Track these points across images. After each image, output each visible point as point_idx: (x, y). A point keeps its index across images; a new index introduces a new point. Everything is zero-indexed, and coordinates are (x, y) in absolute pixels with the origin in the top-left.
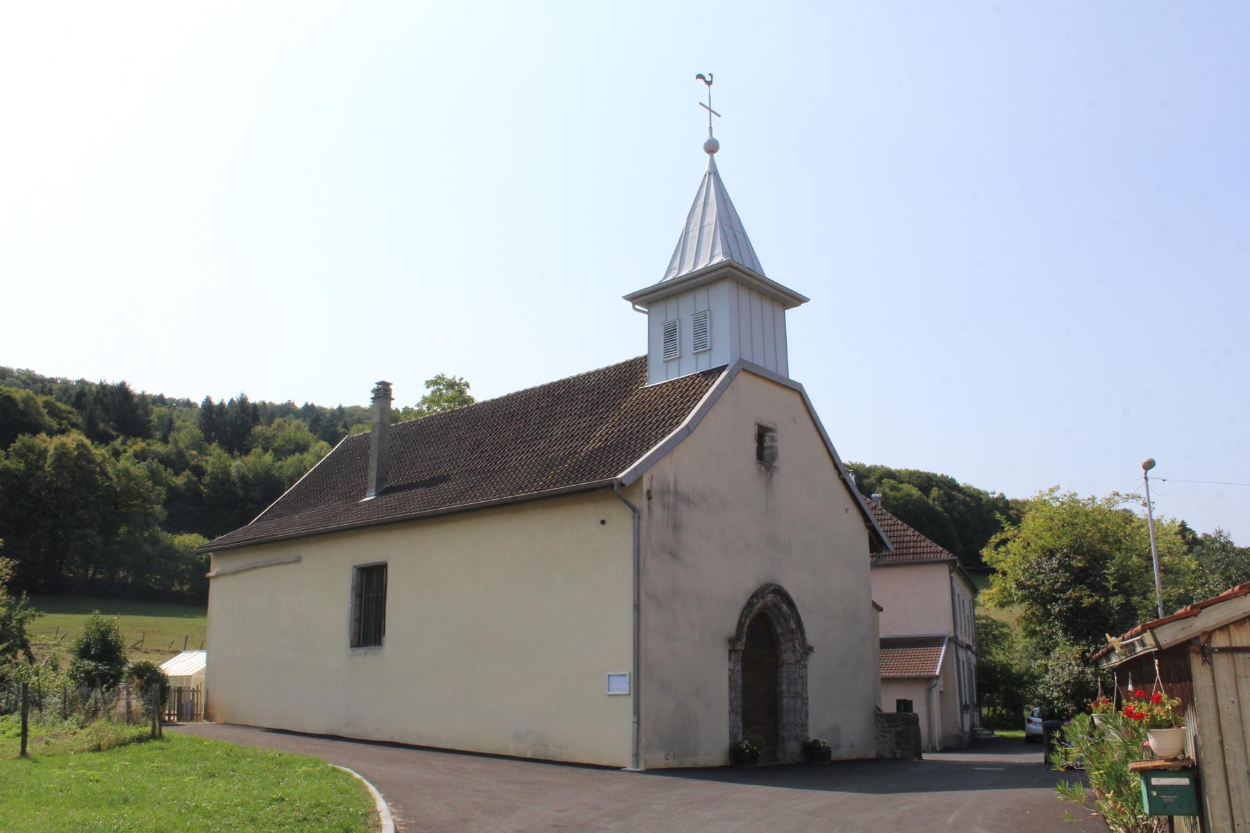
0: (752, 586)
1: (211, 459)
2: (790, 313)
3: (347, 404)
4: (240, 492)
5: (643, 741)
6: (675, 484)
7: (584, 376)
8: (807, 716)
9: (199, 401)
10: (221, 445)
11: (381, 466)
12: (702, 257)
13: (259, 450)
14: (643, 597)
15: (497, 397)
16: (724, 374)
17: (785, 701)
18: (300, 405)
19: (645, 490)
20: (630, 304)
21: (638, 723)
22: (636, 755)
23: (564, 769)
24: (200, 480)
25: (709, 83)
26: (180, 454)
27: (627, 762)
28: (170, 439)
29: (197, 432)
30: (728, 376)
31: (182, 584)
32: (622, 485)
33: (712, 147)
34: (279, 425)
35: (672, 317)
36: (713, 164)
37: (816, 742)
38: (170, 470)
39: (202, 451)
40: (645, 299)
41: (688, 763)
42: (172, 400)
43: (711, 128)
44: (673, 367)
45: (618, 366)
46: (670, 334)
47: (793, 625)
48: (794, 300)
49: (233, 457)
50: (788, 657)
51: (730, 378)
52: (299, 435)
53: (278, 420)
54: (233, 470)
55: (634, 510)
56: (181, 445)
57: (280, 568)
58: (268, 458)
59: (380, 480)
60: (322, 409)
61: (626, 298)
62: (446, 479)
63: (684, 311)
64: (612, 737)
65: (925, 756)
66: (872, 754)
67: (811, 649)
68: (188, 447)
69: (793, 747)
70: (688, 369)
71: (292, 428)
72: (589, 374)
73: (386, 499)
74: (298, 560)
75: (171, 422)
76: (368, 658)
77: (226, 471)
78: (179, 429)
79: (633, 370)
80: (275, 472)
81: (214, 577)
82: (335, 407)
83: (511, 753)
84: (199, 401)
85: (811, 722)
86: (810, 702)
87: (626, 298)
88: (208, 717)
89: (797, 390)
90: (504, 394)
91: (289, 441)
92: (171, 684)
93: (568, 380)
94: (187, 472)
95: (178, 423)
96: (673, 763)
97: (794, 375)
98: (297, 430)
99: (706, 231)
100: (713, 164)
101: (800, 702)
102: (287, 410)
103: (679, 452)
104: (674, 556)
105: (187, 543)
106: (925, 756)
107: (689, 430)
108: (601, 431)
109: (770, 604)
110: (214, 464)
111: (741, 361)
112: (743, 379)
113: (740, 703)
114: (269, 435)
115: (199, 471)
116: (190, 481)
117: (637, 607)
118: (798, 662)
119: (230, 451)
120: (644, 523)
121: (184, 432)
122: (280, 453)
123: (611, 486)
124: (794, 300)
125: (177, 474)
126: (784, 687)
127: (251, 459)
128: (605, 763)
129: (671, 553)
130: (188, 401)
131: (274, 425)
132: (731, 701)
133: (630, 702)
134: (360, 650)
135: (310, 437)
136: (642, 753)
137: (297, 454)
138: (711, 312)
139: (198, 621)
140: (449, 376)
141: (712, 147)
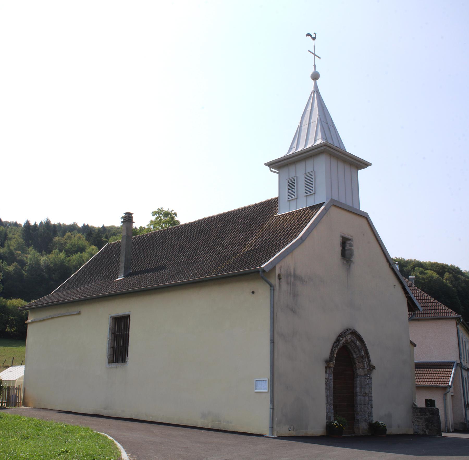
0: (338, 329)
1: (29, 256)
2: (361, 173)
3: (107, 225)
4: (46, 275)
5: (276, 419)
7: (242, 209)
8: (372, 407)
9: (22, 223)
10: (35, 248)
11: (127, 260)
12: (309, 141)
13: (57, 251)
14: (276, 335)
15: (192, 221)
16: (322, 208)
17: (359, 398)
18: (80, 225)
19: (277, 274)
20: (268, 168)
21: (273, 408)
22: (272, 428)
23: (230, 435)
24: (22, 268)
25: (314, 39)
26: (11, 253)
27: (266, 431)
28: (5, 245)
29: (21, 240)
31: (11, 328)
32: (264, 271)
33: (315, 77)
34: (69, 236)
35: (293, 174)
36: (316, 86)
37: (377, 423)
38: (5, 263)
40: (277, 165)
41: (302, 433)
42: (6, 222)
43: (315, 65)
44: (293, 203)
45: (261, 204)
46: (292, 185)
48: (363, 164)
49: (42, 255)
50: (360, 372)
52: (80, 242)
53: (68, 234)
54: (42, 262)
55: (271, 285)
56: (12, 248)
58: (62, 255)
59: (126, 268)
60: (93, 227)
62: (164, 267)
63: (299, 172)
64: (257, 417)
65: (444, 434)
66: (411, 432)
67: (374, 367)
68: (16, 249)
69: (363, 426)
70: (302, 204)
71: (76, 238)
73: (130, 279)
74: (79, 313)
75: (6, 235)
77: (38, 263)
78: (10, 239)
79: (270, 206)
81: (29, 323)
82: (101, 226)
83: (200, 425)
86: (373, 398)
88: (25, 404)
89: (365, 217)
91: (74, 245)
94: (15, 264)
95: (10, 235)
96: (293, 433)
100: (316, 86)
102: (73, 228)
103: (297, 252)
104: (294, 311)
105: (15, 304)
106: (444, 434)
107: (302, 240)
109: (349, 341)
110: (31, 259)
111: (332, 200)
112: (334, 211)
113: (332, 398)
114: (63, 242)
115: (22, 263)
118: (366, 375)
119: (40, 252)
120: (276, 293)
121: (13, 240)
122: (69, 253)
124: (363, 164)
125: (9, 265)
128: (253, 432)
129: (292, 310)
130: (16, 223)
131: (66, 237)
132: (327, 397)
133: (268, 396)
134: (114, 365)
135: (86, 243)
136: (275, 427)
137: (79, 253)
138: (315, 172)
140: (165, 209)
141: (315, 77)
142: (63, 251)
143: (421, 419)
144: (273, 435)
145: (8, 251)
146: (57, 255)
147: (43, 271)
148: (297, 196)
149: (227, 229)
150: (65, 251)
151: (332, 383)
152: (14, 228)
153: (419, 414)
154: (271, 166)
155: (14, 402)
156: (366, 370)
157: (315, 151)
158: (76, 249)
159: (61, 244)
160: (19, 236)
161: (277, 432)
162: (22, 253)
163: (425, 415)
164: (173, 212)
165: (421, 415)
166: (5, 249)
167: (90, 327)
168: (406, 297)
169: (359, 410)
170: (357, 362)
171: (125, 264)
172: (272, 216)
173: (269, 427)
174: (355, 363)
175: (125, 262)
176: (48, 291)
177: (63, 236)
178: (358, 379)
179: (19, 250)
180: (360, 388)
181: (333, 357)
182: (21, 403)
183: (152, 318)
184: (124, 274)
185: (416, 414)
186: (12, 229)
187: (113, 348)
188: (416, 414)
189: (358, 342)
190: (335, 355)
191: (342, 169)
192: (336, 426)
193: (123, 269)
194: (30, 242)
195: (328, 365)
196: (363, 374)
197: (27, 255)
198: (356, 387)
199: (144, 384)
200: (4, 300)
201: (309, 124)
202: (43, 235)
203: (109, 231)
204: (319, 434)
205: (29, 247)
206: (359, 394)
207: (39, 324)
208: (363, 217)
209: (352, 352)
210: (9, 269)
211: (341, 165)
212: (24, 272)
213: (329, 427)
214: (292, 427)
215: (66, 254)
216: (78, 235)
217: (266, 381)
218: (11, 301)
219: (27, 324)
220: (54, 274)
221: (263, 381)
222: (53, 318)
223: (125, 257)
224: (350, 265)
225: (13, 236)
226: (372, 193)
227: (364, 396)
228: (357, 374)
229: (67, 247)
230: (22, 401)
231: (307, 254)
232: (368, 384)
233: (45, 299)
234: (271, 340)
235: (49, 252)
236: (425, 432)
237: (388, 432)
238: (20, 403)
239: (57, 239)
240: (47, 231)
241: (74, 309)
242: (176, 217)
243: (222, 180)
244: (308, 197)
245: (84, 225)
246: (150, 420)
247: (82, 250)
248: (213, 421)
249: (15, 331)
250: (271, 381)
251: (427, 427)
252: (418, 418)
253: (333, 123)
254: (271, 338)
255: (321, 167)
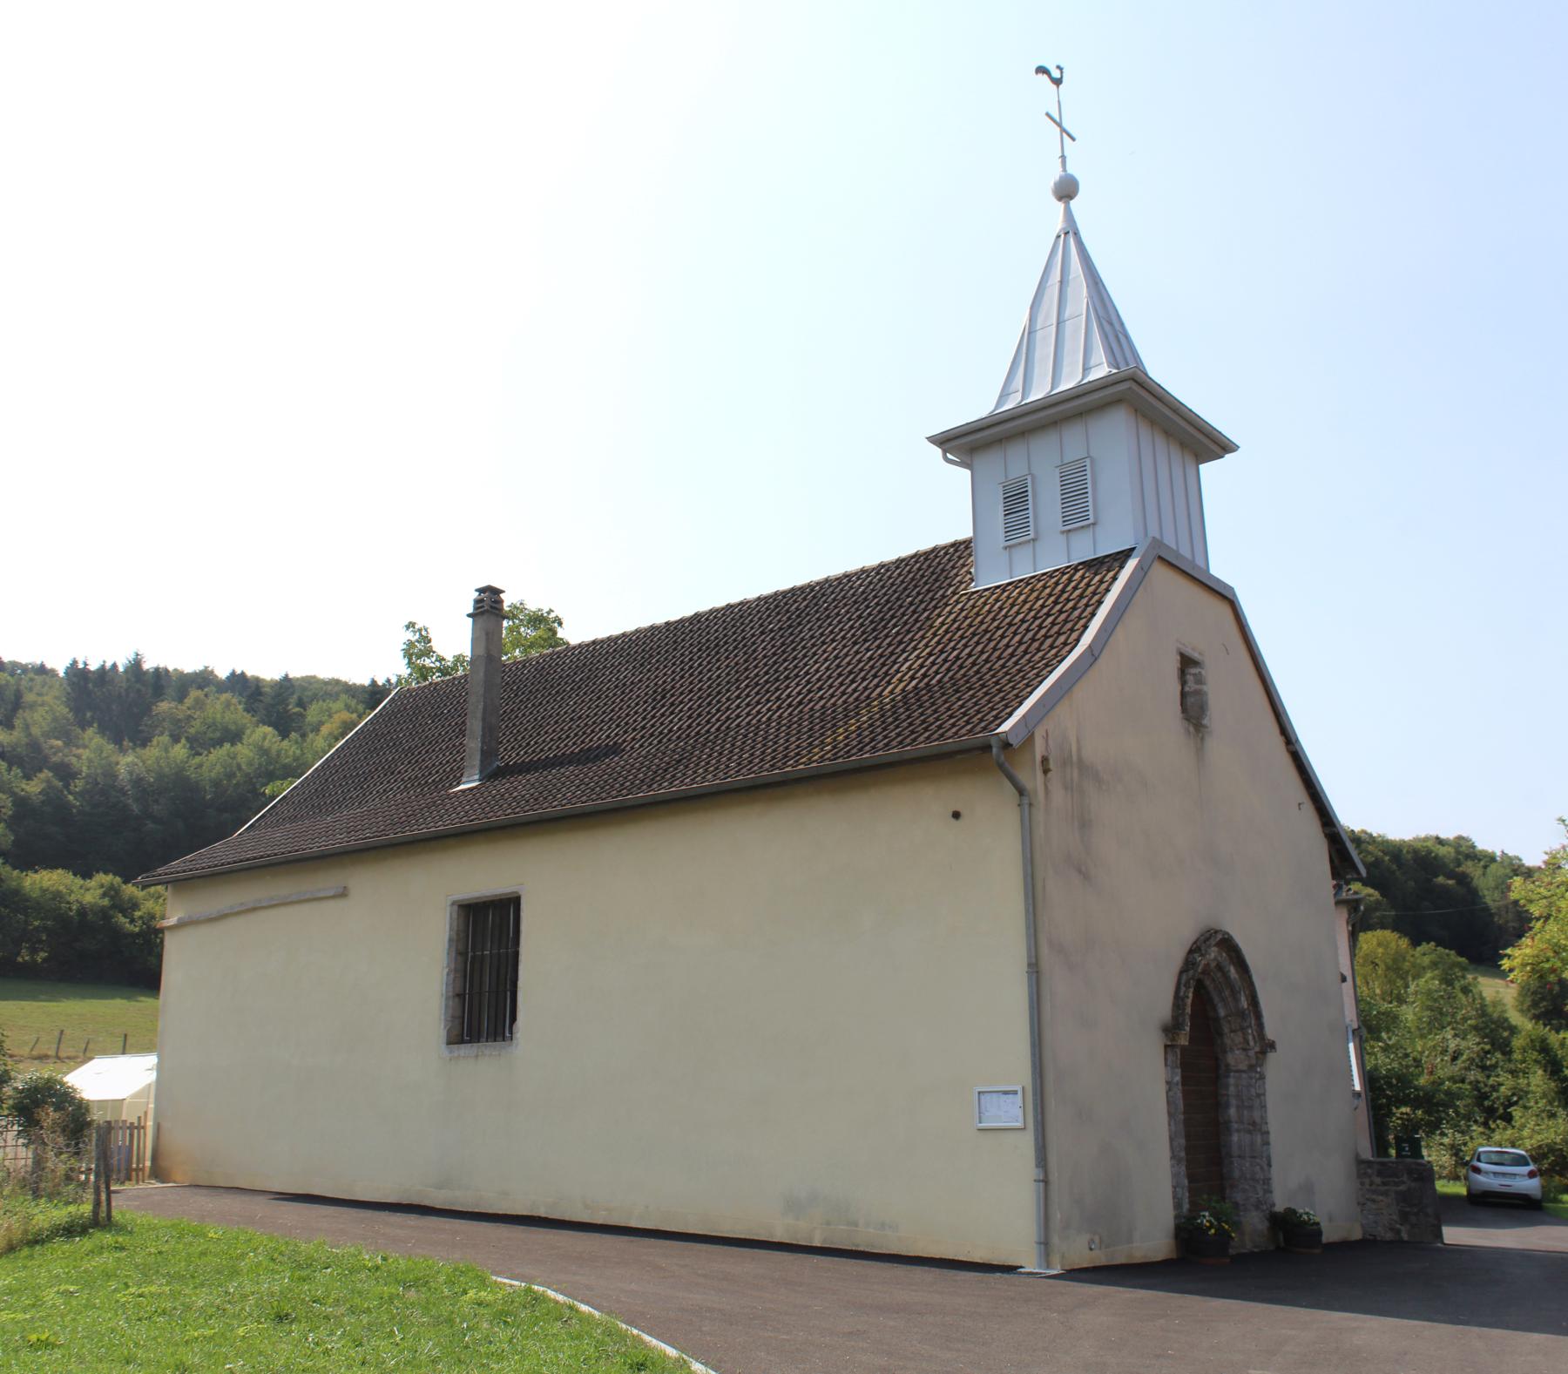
0: (1186, 935)
1: (85, 754)
2: (1210, 471)
3: (296, 673)
4: (136, 808)
5: (1057, 1217)
6: (1079, 750)
7: (839, 579)
8: (1269, 1165)
9: (60, 666)
10: (102, 730)
11: (489, 732)
12: (1066, 370)
13: (165, 739)
14: (1045, 950)
16: (1131, 564)
17: (1235, 1138)
18: (222, 673)
19: (1038, 758)
20: (938, 451)
21: (1046, 1182)
22: (1045, 1244)
23: (918, 1272)
24: (67, 786)
26: (34, 746)
28: (17, 722)
29: (63, 710)
30: (1139, 567)
31: (34, 951)
32: (1006, 745)
33: (1066, 190)
34: (197, 700)
35: (1017, 469)
36: (1069, 216)
37: (1291, 1212)
38: (16, 771)
39: (70, 741)
40: (963, 444)
42: (15, 665)
43: (1063, 157)
46: (1016, 500)
47: (1244, 1003)
48: (1217, 446)
49: (123, 751)
51: (1141, 571)
52: (229, 717)
53: (194, 694)
54: (122, 771)
55: (1021, 792)
56: (35, 731)
57: (305, 909)
58: (180, 751)
59: (487, 754)
60: (257, 680)
61: (934, 440)
62: (615, 750)
63: (1041, 465)
64: (997, 1210)
65: (1454, 1235)
66: (1357, 1235)
68: (47, 735)
69: (1255, 1222)
71: (219, 707)
72: (793, 591)
73: (503, 786)
74: (343, 894)
75: (18, 695)
76: (482, 1065)
77: (111, 774)
78: (32, 706)
79: (938, 568)
80: (191, 774)
81: (170, 928)
82: (277, 676)
83: (779, 1236)
84: (60, 666)
85: (1276, 1173)
87: (934, 440)
88: (158, 1173)
89: (1225, 597)
90: (689, 612)
91: (212, 725)
92: (96, 1116)
93: (810, 587)
94: (46, 774)
95: (29, 697)
96: (1100, 1258)
97: (1220, 568)
98: (233, 712)
99: (1069, 327)
100: (1069, 216)
101: (1259, 1139)
102: (204, 679)
103: (1081, 692)
104: (1085, 875)
105: (46, 884)
106: (1454, 1235)
107: (1093, 654)
108: (908, 663)
109: (1213, 965)
110: (90, 760)
111: (1157, 543)
112: (1159, 571)
113: (1183, 1141)
114: (181, 716)
115: (66, 773)
116: (50, 786)
117: (1035, 969)
118: (1252, 1068)
119: (118, 741)
120: (1039, 815)
121: (41, 711)
122: (199, 744)
123: (987, 748)
124: (1217, 446)
125: (28, 777)
126: (1232, 1111)
127: (152, 753)
128: (978, 1256)
129: (1080, 871)
130: (42, 666)
131: (189, 701)
133: (1027, 1143)
134: (464, 1050)
135: (246, 719)
137: (227, 746)
138: (1093, 462)
139: (146, 1002)
140: (532, 606)
141: (1066, 190)
142: (183, 741)
143: (1385, 1194)
144: (1048, 1267)
145: (25, 740)
146: (166, 751)
147: (125, 794)
148: (1036, 532)
149: (806, 634)
150: (188, 739)
151: (1180, 1095)
152: (39, 679)
153: (1378, 1180)
154: (947, 446)
155: (123, 1167)
156: (1251, 1053)
157: (1096, 396)
158: (218, 734)
159: (177, 722)
160: (56, 698)
161: (1063, 1257)
162: (67, 744)
163: (1397, 1184)
164: (552, 615)
165: (1384, 1184)
166: (15, 733)
167: (396, 930)
168: (1326, 835)
169: (1236, 1174)
170: (1226, 1030)
171: (483, 742)
172: (954, 593)
173: (1035, 1238)
174: (1221, 1034)
175: (483, 736)
176: (223, 832)
177: (181, 700)
178: (1232, 1081)
179: (57, 738)
180: (1238, 1107)
181: (1183, 1014)
182: (147, 1171)
183: (588, 904)
184: (481, 772)
185: (1367, 1181)
186: (32, 680)
187: (460, 996)
188: (1367, 1181)
189: (1232, 969)
190: (1188, 1010)
191: (1164, 455)
192: (1209, 1228)
193: (478, 757)
194: (89, 714)
195: (1173, 1039)
196: (1243, 1067)
197: (80, 751)
198: (1227, 1106)
199: (575, 1107)
200: (16, 873)
201: (1060, 323)
202: (123, 699)
203: (304, 689)
204: (1160, 1257)
205: (84, 730)
206: (1235, 1126)
207: (204, 931)
208: (1224, 597)
209: (1216, 999)
210: (28, 788)
211: (1161, 442)
212: (71, 798)
213: (1188, 1236)
214: (1097, 1239)
215: (191, 748)
216: (225, 696)
217: (1015, 1093)
218: (37, 877)
219: (162, 930)
220: (156, 801)
221: (1006, 1093)
222: (254, 909)
223: (484, 719)
224: (1202, 739)
225: (40, 700)
226: (1243, 526)
227: (1250, 1132)
228: (1227, 1065)
229: (192, 731)
230: (148, 1164)
231: (1085, 702)
232: (1258, 1096)
233: (219, 852)
234: (1029, 965)
235: (145, 743)
236: (1398, 1232)
237: (1327, 1237)
238: (143, 1170)
239: (164, 706)
240: (138, 686)
241: (326, 881)
242: (559, 630)
243: (802, 480)
244: (1075, 537)
245: (233, 674)
246: (600, 1221)
247: (234, 736)
248: (828, 1224)
249: (44, 960)
250: (1035, 1094)
251: (1404, 1217)
252: (1374, 1192)
253: (1122, 324)
254: (1029, 957)
255: (1114, 444)
